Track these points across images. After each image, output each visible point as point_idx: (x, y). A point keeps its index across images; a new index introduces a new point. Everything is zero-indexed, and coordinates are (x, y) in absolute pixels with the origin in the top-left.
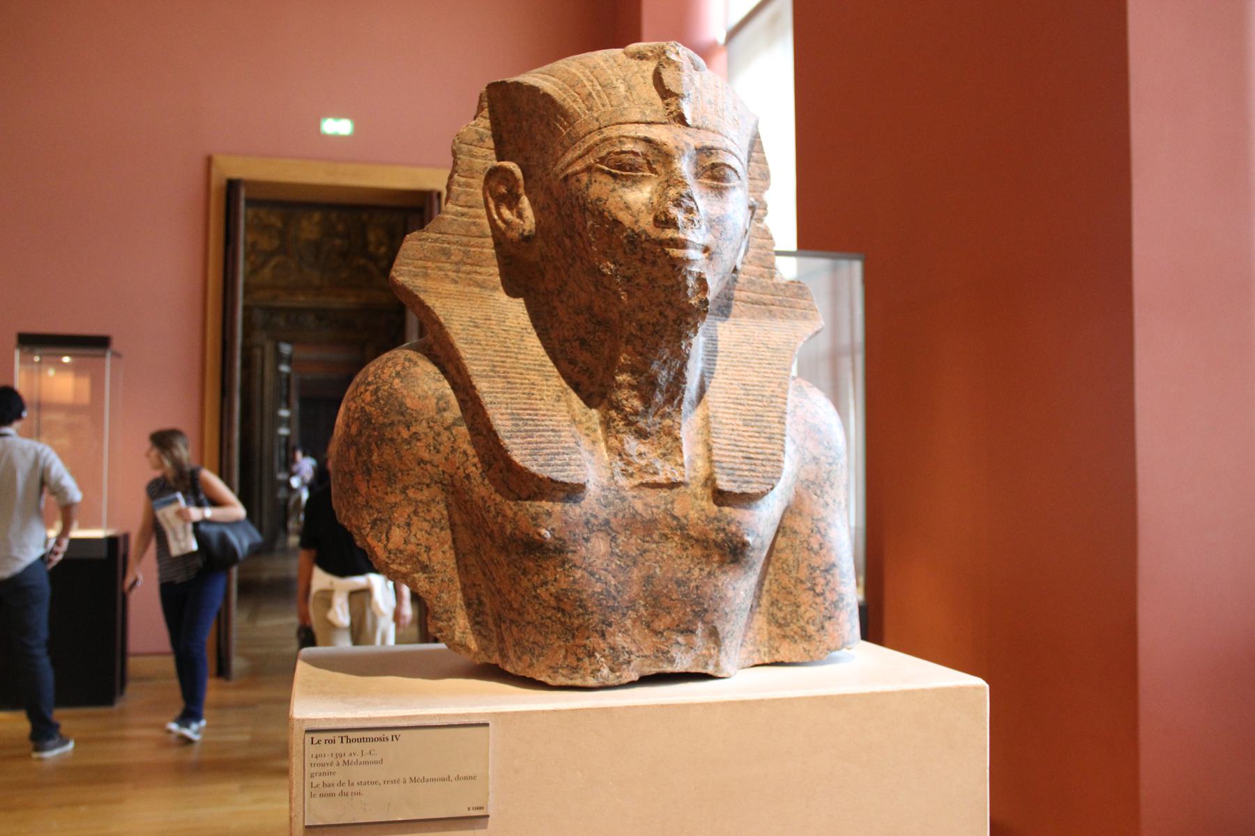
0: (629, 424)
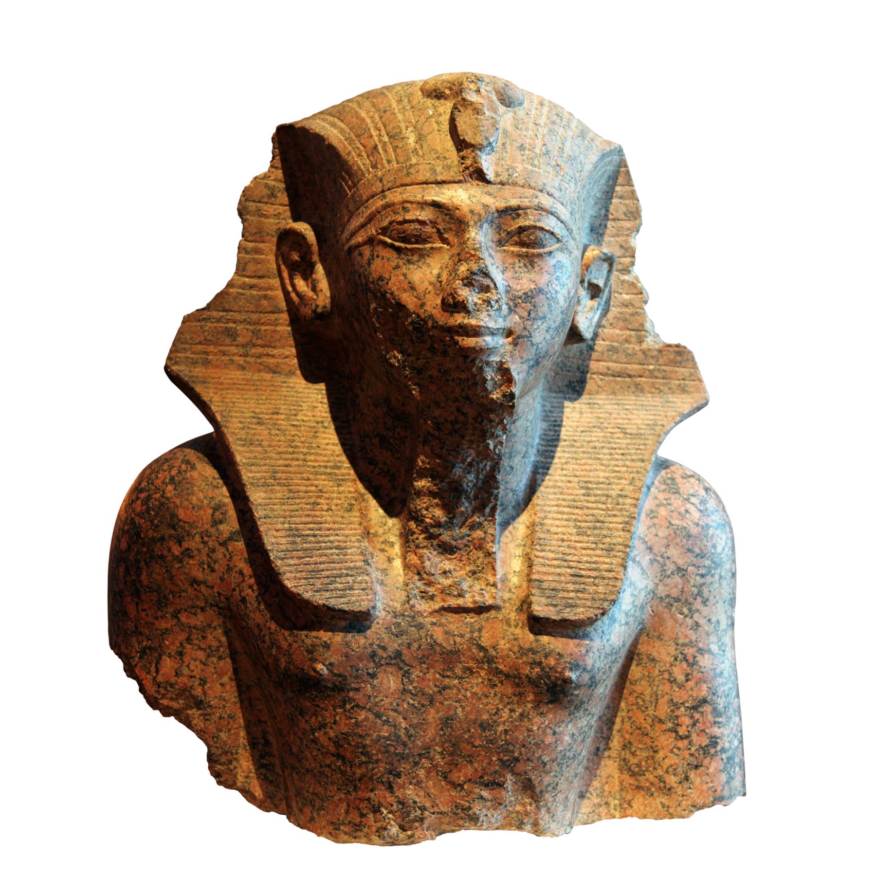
0: (431, 537)
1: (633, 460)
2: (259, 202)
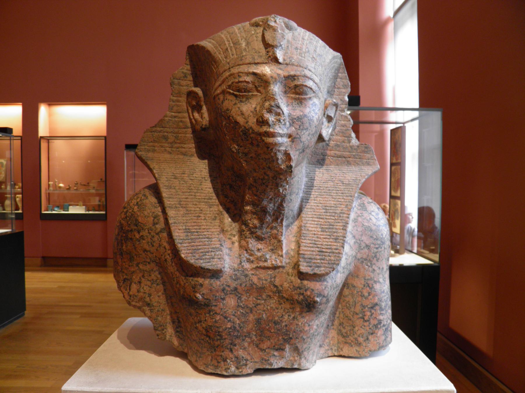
0: (252, 233)
1: (347, 196)
2: (179, 79)
